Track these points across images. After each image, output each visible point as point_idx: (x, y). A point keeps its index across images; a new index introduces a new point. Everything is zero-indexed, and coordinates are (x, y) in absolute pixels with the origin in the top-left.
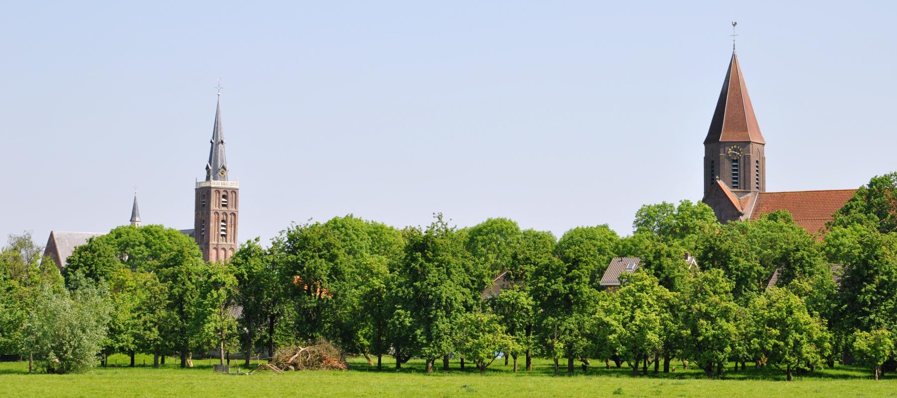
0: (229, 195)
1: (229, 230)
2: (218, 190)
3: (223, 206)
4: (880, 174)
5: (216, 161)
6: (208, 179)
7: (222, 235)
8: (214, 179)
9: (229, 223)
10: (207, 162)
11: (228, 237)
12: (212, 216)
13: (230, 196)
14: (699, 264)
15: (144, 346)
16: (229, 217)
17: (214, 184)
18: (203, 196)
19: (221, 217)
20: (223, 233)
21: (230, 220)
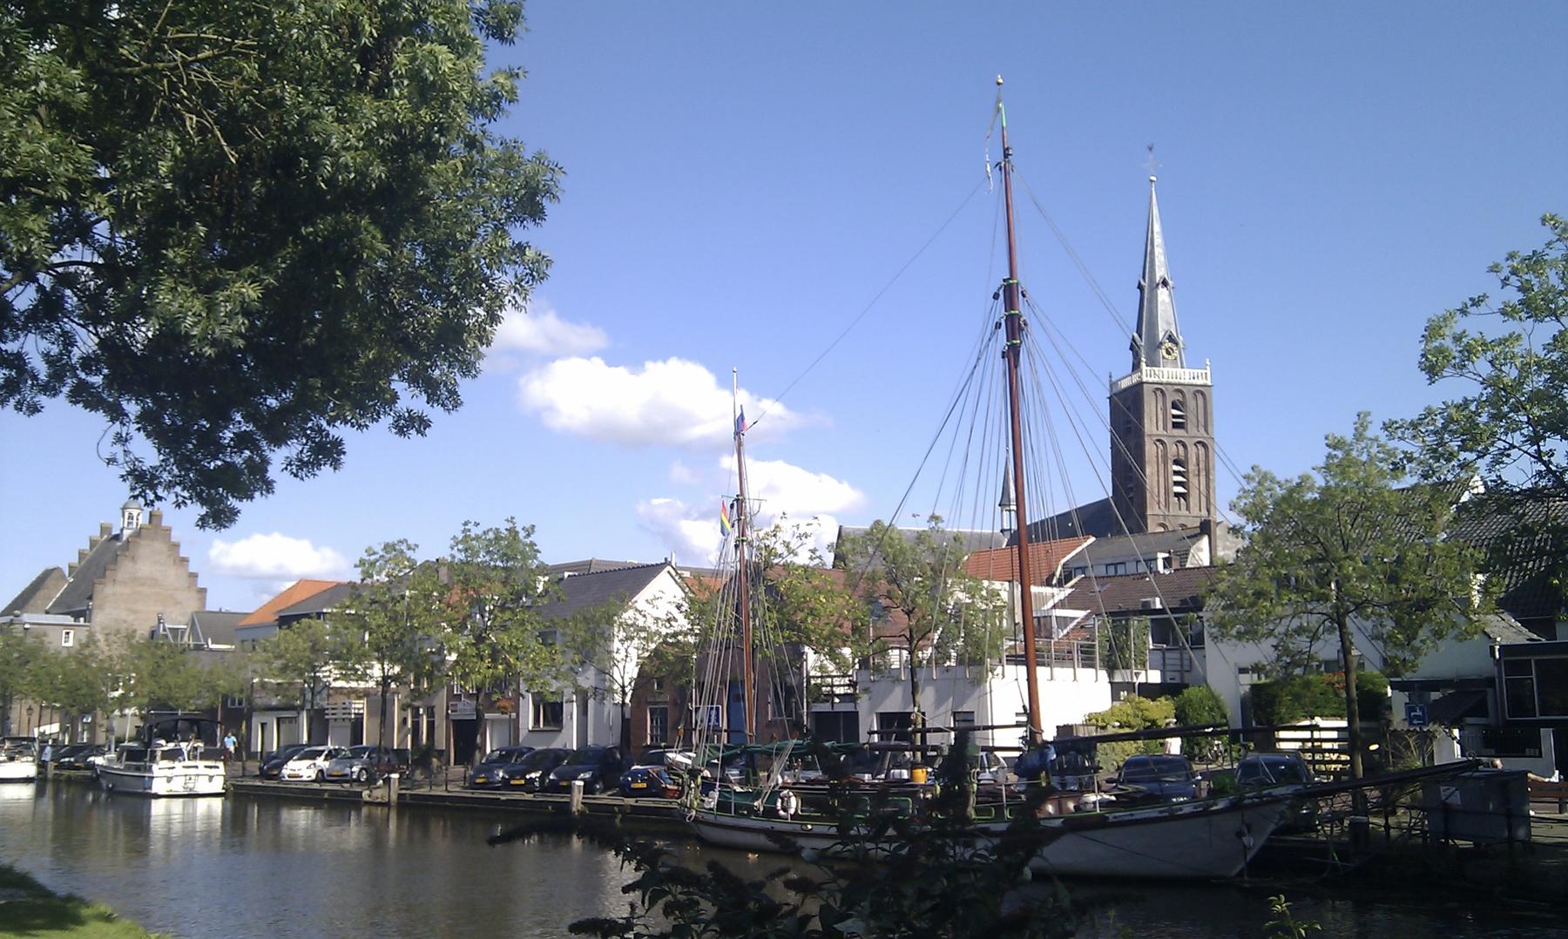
0: (1187, 406)
1: (1193, 481)
2: (1160, 390)
3: (1175, 425)
4: (1071, 723)
5: (1153, 325)
6: (1136, 367)
7: (1177, 495)
8: (1152, 363)
9: (1192, 467)
10: (1138, 277)
11: (1193, 500)
12: (1150, 449)
13: (1191, 403)
14: (666, 672)
15: (305, 464)
16: (1192, 450)
17: (1147, 374)
18: (1126, 409)
19: (1172, 450)
20: (1179, 478)
21: (1192, 466)
